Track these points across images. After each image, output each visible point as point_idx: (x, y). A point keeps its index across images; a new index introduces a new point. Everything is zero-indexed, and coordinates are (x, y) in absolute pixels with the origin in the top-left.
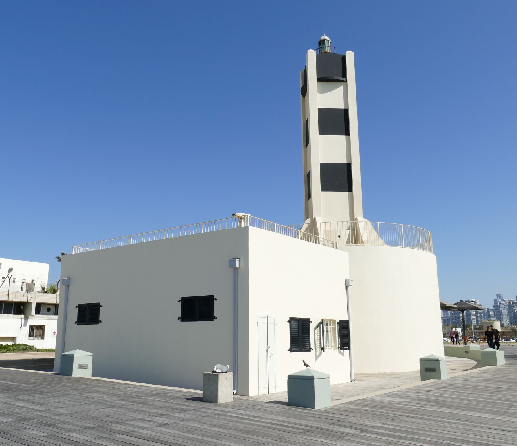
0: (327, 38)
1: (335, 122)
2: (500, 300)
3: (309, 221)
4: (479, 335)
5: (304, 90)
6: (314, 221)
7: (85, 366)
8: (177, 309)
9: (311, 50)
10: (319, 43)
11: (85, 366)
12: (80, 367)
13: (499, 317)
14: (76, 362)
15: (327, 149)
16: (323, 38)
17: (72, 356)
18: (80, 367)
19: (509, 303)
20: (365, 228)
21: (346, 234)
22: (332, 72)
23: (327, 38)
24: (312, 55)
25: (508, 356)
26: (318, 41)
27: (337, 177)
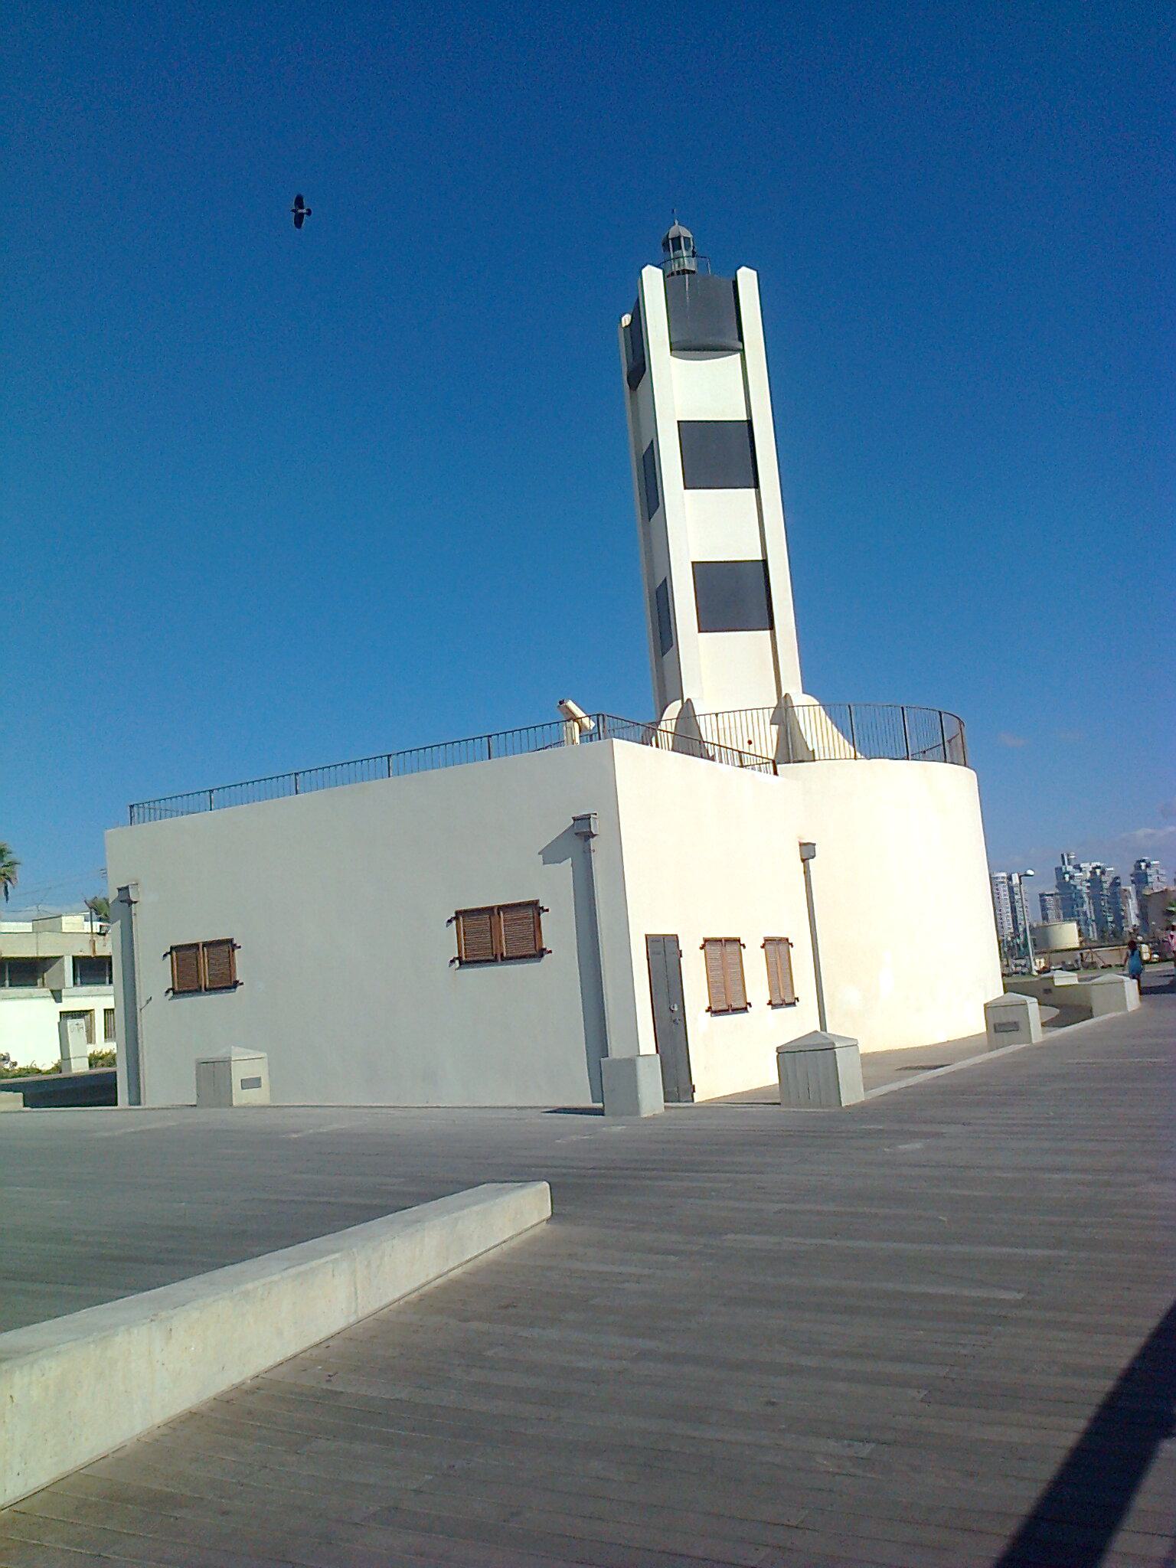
0: (685, 233)
1: (719, 455)
2: (1070, 868)
3: (674, 709)
4: (1077, 961)
5: (639, 370)
6: (688, 705)
7: (255, 1083)
8: (448, 943)
9: (649, 267)
10: (665, 245)
11: (255, 1083)
12: (246, 1084)
13: (1069, 912)
14: (239, 1072)
15: (705, 526)
16: (673, 232)
17: (227, 1062)
18: (246, 1084)
19: (1093, 873)
20: (814, 723)
21: (767, 740)
22: (706, 333)
23: (685, 233)
24: (653, 280)
25: (1000, 1025)
26: (661, 241)
27: (734, 596)
